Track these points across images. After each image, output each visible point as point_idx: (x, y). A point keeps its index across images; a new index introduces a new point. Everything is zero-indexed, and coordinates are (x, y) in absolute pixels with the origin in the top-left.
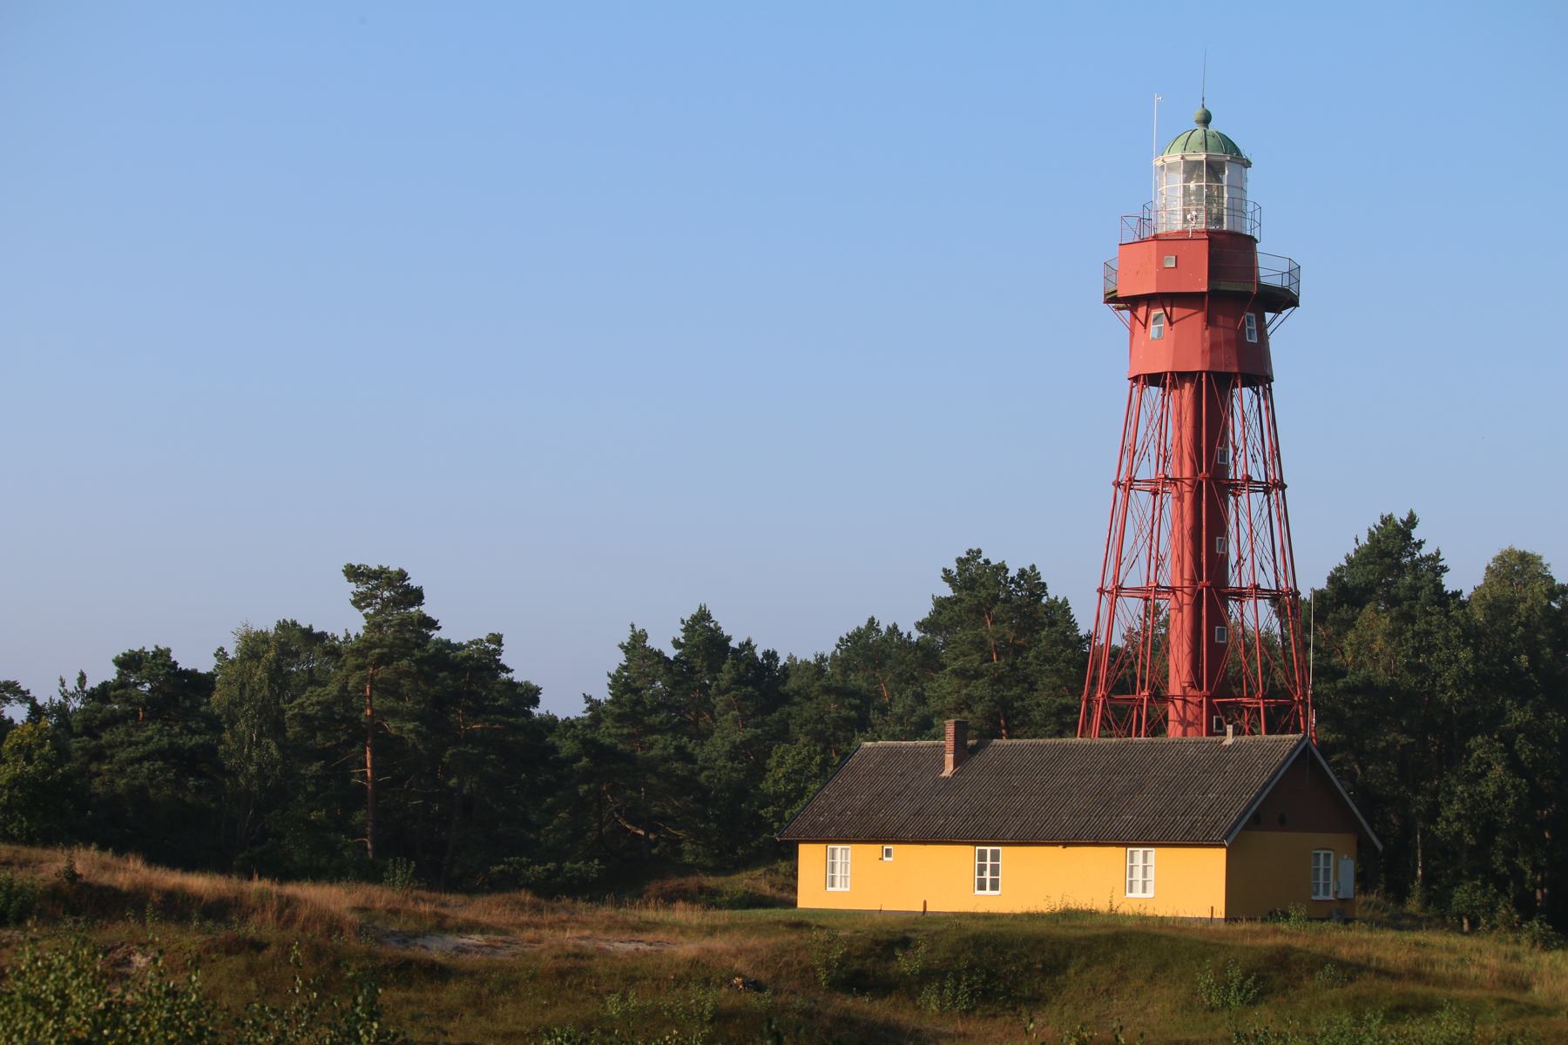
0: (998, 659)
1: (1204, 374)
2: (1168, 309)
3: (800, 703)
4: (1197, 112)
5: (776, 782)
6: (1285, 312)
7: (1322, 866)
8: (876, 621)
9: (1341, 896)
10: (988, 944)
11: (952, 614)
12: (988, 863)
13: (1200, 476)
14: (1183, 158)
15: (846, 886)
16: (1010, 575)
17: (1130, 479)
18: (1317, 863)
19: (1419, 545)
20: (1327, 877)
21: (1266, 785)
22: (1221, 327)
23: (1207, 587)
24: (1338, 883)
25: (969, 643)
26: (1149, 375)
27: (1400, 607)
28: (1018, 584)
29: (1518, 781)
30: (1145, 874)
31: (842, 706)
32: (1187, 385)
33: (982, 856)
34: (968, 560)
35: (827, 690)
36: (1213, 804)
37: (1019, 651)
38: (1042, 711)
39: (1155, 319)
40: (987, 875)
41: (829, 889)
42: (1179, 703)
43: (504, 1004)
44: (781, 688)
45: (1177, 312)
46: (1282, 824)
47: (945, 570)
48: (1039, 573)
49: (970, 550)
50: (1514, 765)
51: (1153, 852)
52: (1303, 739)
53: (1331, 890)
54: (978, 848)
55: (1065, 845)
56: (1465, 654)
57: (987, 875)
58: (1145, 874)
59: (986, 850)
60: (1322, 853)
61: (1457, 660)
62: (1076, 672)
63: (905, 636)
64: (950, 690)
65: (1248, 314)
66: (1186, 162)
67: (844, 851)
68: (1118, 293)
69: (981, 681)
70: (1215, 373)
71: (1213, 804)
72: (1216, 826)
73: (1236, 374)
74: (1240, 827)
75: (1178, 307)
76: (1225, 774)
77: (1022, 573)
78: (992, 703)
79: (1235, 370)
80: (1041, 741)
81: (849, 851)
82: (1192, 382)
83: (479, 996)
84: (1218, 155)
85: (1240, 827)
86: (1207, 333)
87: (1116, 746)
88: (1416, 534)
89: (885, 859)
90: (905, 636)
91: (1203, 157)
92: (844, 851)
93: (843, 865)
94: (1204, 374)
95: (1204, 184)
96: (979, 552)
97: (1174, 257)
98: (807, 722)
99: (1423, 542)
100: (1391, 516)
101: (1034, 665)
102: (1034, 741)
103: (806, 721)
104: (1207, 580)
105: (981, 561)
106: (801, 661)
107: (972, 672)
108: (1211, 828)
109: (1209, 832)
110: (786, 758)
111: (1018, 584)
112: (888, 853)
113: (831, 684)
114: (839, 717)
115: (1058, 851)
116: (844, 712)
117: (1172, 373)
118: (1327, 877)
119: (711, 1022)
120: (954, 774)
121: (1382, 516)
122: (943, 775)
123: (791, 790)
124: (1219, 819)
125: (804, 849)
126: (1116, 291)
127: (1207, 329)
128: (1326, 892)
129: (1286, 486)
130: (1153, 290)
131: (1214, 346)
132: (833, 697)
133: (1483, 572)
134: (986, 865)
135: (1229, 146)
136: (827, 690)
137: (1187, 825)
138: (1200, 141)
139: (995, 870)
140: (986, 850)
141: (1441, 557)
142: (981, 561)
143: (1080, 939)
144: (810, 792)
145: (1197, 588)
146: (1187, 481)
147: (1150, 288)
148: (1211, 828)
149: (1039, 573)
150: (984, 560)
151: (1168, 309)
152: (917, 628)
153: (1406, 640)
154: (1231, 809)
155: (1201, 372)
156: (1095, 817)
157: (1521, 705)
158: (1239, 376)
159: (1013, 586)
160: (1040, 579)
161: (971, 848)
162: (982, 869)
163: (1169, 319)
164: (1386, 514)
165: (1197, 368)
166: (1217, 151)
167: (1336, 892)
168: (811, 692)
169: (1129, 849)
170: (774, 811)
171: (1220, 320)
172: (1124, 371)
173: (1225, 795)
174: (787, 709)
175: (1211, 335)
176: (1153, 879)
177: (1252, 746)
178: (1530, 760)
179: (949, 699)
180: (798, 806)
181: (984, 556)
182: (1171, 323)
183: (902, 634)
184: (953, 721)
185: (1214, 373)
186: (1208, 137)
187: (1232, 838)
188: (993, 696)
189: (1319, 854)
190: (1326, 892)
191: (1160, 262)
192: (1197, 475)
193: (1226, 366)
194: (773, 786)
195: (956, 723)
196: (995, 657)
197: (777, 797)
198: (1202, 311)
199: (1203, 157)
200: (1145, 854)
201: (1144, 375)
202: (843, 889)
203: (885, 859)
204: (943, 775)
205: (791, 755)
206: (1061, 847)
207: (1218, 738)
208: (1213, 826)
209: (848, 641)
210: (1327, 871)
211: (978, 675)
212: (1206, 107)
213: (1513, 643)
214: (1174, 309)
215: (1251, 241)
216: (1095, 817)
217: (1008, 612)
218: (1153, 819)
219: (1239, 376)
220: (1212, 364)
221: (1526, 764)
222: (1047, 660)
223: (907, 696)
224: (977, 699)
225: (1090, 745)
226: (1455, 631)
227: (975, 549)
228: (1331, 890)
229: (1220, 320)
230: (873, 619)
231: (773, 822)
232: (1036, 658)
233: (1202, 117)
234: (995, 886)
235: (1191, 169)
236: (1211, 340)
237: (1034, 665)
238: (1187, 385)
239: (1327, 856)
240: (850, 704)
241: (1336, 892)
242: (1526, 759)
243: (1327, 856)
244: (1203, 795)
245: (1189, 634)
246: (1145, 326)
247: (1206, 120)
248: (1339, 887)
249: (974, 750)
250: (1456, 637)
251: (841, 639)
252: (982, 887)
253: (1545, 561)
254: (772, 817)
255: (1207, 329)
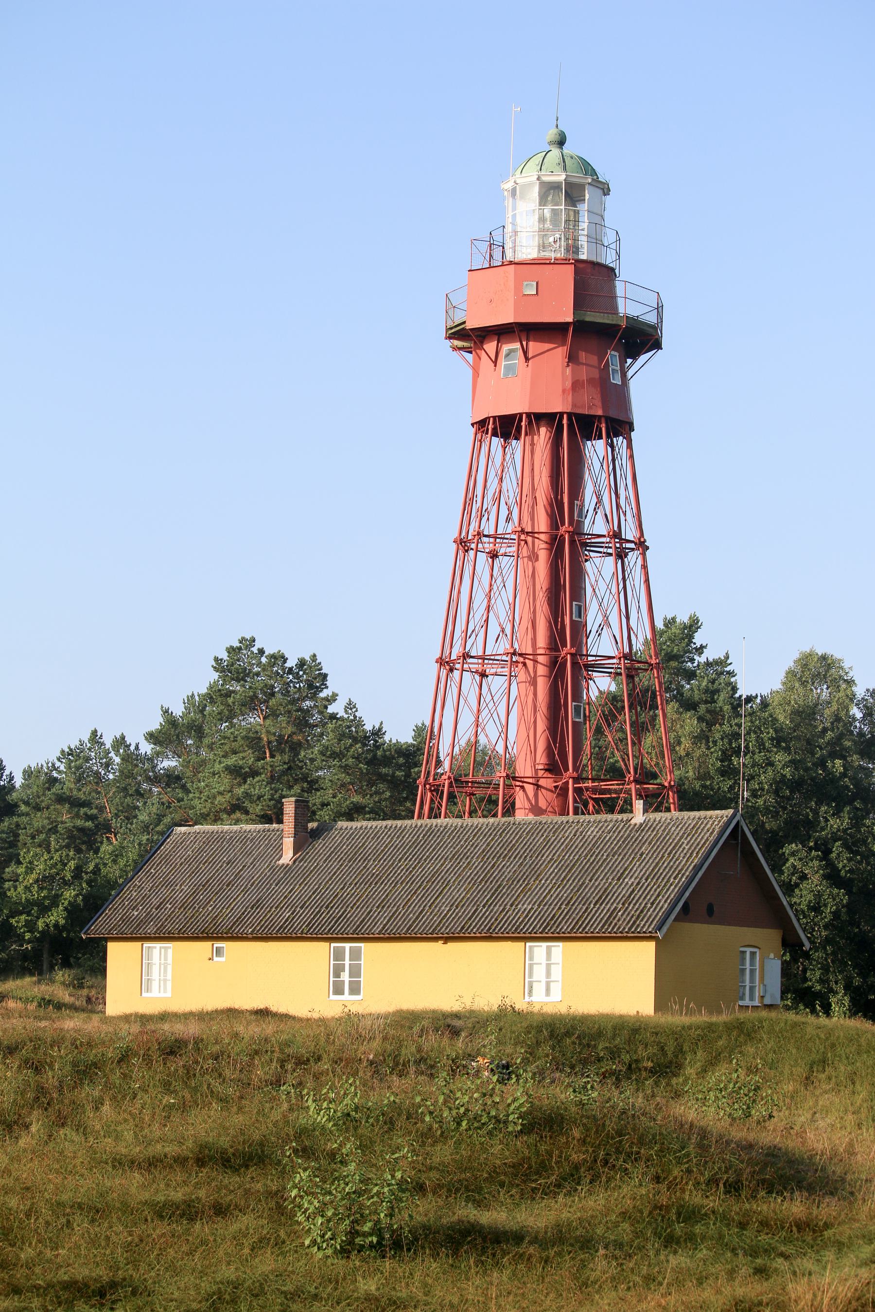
0: (272, 756)
1: (565, 416)
2: (524, 343)
3: (27, 814)
4: (552, 134)
5: (27, 889)
6: (643, 358)
7: (748, 965)
8: (99, 734)
9: (767, 1001)
10: (568, 1034)
11: (222, 707)
12: (347, 962)
13: (563, 529)
14: (538, 179)
15: (165, 991)
16: (288, 665)
17: (479, 533)
18: (743, 963)
19: (700, 650)
20: (752, 980)
21: (697, 868)
22: (583, 364)
23: (571, 654)
24: (765, 986)
25: (243, 738)
26: (499, 417)
27: (696, 710)
28: (297, 676)
29: (836, 891)
30: (548, 974)
31: (77, 816)
32: (543, 430)
33: (339, 955)
34: (240, 649)
35: (61, 799)
36: (633, 891)
37: (295, 748)
38: (332, 810)
39: (507, 355)
40: (345, 977)
41: (144, 994)
42: (530, 789)
43: (98, 1105)
44: (8, 798)
45: (534, 347)
46: (710, 914)
47: (216, 659)
48: (320, 663)
49: (243, 638)
50: (833, 877)
51: (558, 948)
52: (734, 816)
53: (757, 994)
54: (333, 945)
55: (447, 940)
56: (780, 758)
57: (345, 977)
58: (548, 974)
59: (344, 947)
60: (748, 950)
61: (771, 764)
62: (367, 769)
63: (132, 748)
64: (222, 789)
65: (613, 353)
66: (543, 184)
67: (163, 950)
68: (466, 324)
69: (257, 779)
70: (578, 416)
71: (633, 891)
72: (642, 915)
73: (600, 417)
74: (673, 917)
75: (534, 341)
76: (641, 855)
77: (302, 663)
78: (272, 802)
79: (600, 412)
80: (399, 823)
81: (170, 951)
82: (550, 425)
83: (41, 1090)
84: (578, 177)
85: (673, 917)
86: (568, 371)
87: (495, 827)
88: (699, 639)
89: (215, 959)
90: (132, 748)
91: (562, 178)
92: (163, 950)
93: (162, 966)
94: (565, 416)
95: (563, 207)
96: (253, 640)
97: (535, 284)
98: (39, 832)
99: (705, 647)
100: (674, 619)
101: (319, 760)
102: (389, 823)
103: (37, 831)
104: (572, 646)
105: (255, 650)
106: (28, 774)
107: (247, 769)
108: (637, 918)
109: (635, 922)
110: (35, 863)
111: (297, 676)
112: (219, 952)
113: (64, 793)
114: (74, 827)
115: (437, 947)
116: (79, 823)
117: (528, 415)
118: (752, 980)
119: (526, 1130)
120: (295, 862)
121: (666, 619)
122: (281, 862)
123: (44, 897)
124: (645, 907)
125: (114, 949)
126: (464, 323)
127: (568, 366)
128: (752, 998)
129: (648, 548)
130: (511, 320)
131: (576, 385)
132: (67, 806)
133: (782, 676)
134: (350, 961)
135: (587, 168)
136: (61, 799)
137: (605, 914)
138: (557, 161)
139: (355, 972)
140: (344, 947)
141: (729, 662)
142: (255, 650)
143: (690, 1028)
144: (65, 899)
145: (557, 657)
146: (542, 537)
147: (507, 317)
148: (637, 918)
149: (320, 663)
150: (259, 649)
151: (524, 343)
152: (146, 739)
153: (715, 742)
154: (658, 895)
155: (561, 414)
156: (484, 906)
157: (837, 813)
158: (603, 420)
159: (291, 677)
160: (320, 669)
161: (324, 945)
162: (338, 971)
163: (525, 353)
164: (669, 617)
165: (557, 408)
166: (580, 173)
167: (762, 997)
168: (42, 801)
169: (528, 944)
170: (26, 921)
171: (582, 355)
172: (467, 417)
173: (646, 880)
174: (15, 819)
175: (573, 371)
176: (560, 978)
177: (669, 824)
178: (847, 869)
179: (219, 798)
180: (52, 915)
181: (258, 645)
182: (527, 359)
183: (130, 745)
184: (293, 799)
185: (576, 415)
186: (565, 157)
187: (665, 929)
188: (272, 795)
189: (745, 952)
190: (752, 998)
191: (518, 288)
192: (558, 529)
193: (590, 408)
194: (25, 893)
195: (296, 801)
196: (268, 755)
197: (30, 903)
198: (563, 345)
199: (562, 178)
200: (549, 949)
201: (494, 417)
202: (162, 995)
203: (215, 959)
204: (281, 862)
205: (42, 859)
206: (441, 942)
207: (625, 816)
208: (639, 916)
209: (69, 754)
210: (752, 972)
211: (254, 773)
212: (561, 127)
213: (821, 749)
214: (531, 343)
215: (609, 273)
216: (484, 906)
217: (287, 705)
218: (560, 908)
219: (603, 420)
220: (574, 405)
221: (843, 873)
222: (335, 755)
223: (153, 804)
224: (255, 798)
225: (461, 827)
226: (768, 733)
227: (248, 637)
228: (757, 994)
229: (582, 355)
230: (96, 731)
231: (24, 933)
232: (322, 753)
233: (557, 138)
234: (355, 989)
235: (548, 190)
236: (573, 378)
237: (319, 760)
238: (543, 430)
239: (753, 954)
240: (86, 814)
241: (762, 997)
242: (844, 867)
243: (753, 954)
244: (619, 879)
245: (545, 711)
246: (495, 363)
247: (561, 142)
248: (765, 991)
249: (315, 834)
250: (769, 739)
251: (63, 752)
252: (338, 990)
253: (846, 665)
254: (23, 926)
255: (568, 366)
